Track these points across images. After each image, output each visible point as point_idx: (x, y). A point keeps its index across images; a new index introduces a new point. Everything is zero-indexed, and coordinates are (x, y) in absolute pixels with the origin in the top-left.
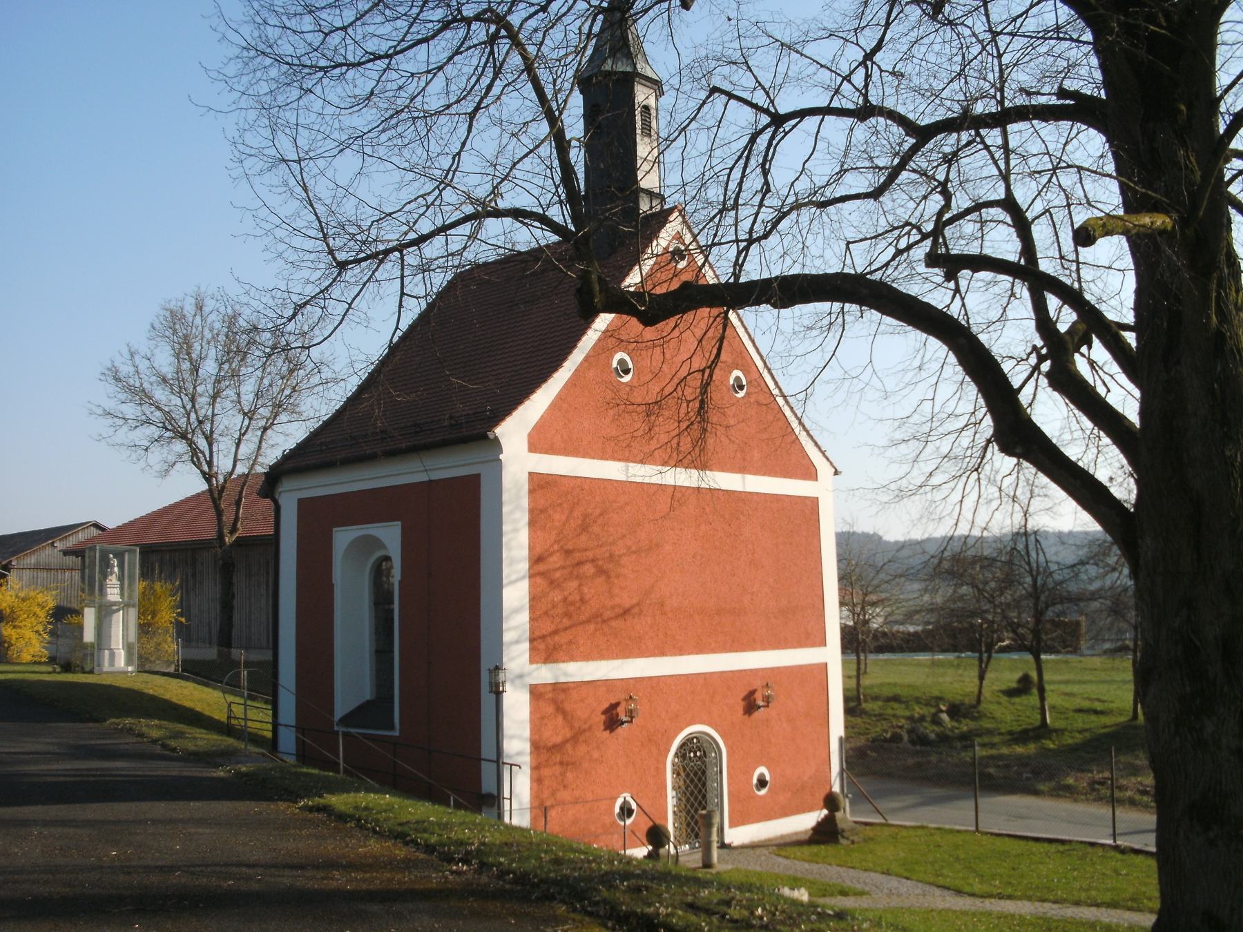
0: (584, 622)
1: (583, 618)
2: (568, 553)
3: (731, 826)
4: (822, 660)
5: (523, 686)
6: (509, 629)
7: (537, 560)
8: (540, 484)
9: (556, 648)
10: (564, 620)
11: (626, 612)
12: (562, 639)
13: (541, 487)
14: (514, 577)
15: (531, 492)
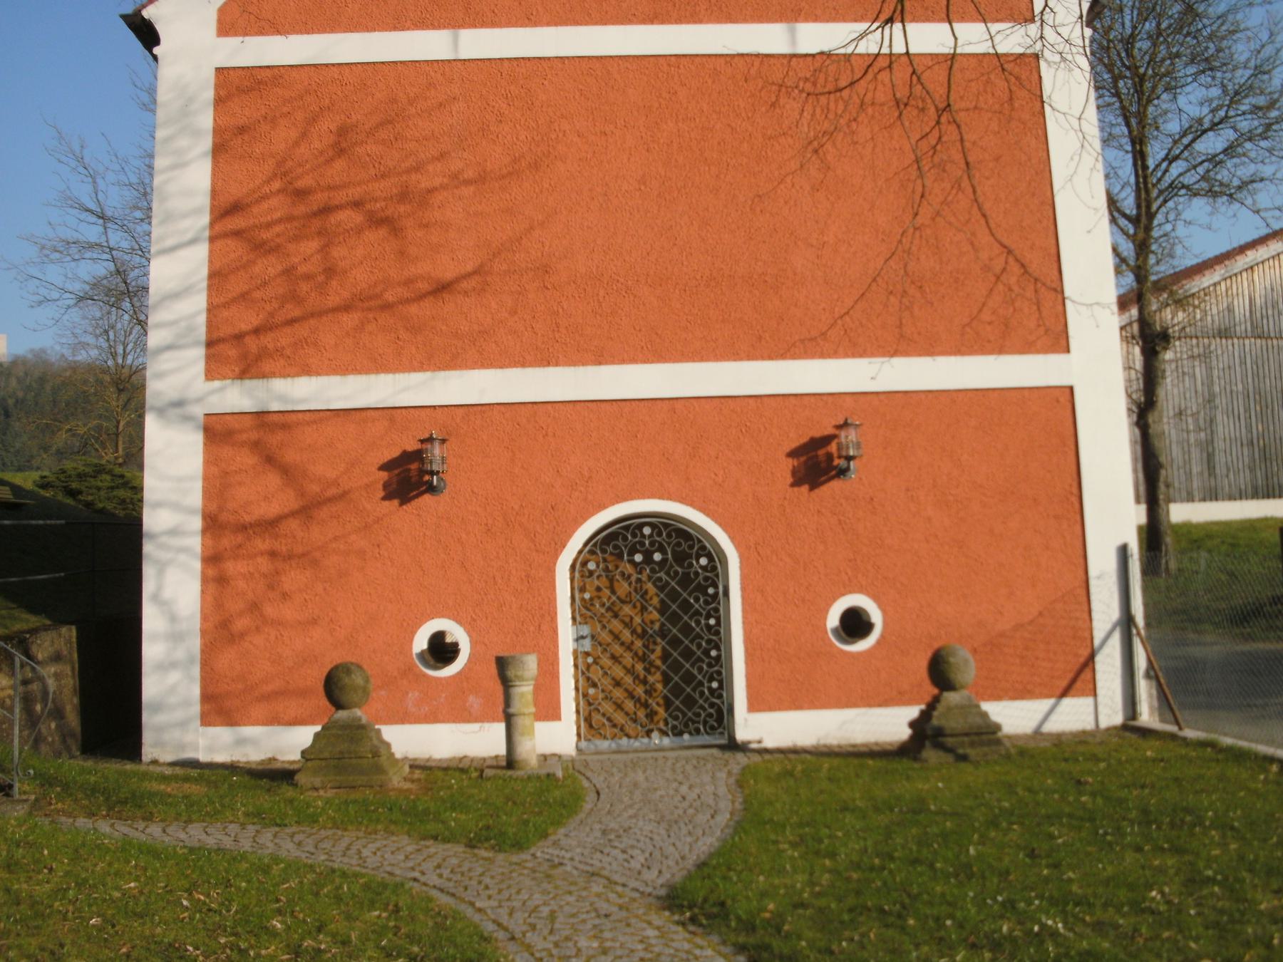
0: (335, 310)
1: (333, 300)
2: (301, 194)
3: (754, 706)
4: (233, 42)
5: (187, 418)
6: (160, 325)
7: (226, 211)
8: (1055, 338)
9: (263, 354)
10: (289, 306)
11: (442, 289)
12: (284, 338)
13: (242, 91)
14: (170, 242)
15: (219, 102)
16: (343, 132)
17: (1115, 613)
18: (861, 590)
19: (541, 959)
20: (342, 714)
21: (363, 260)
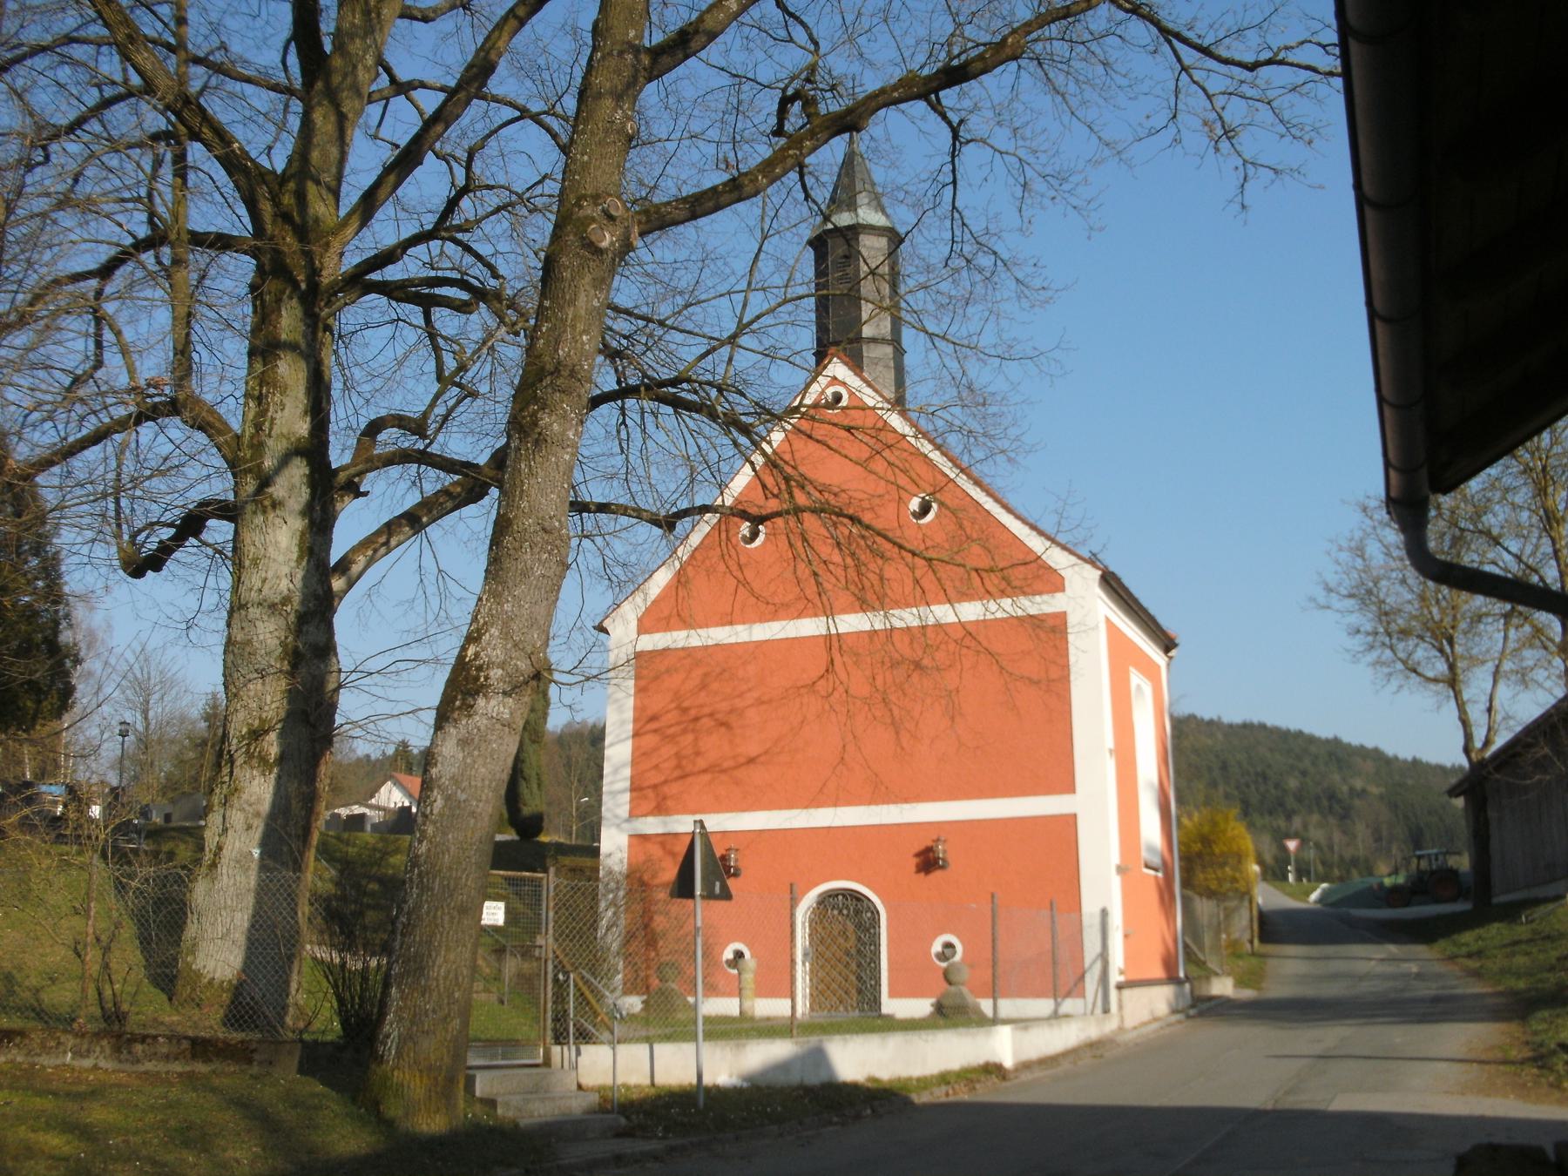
2: (685, 710)
3: (892, 994)
16: (706, 675)
17: (1098, 949)
18: (952, 932)
19: (2, 873)
20: (953, 989)
21: (714, 746)
